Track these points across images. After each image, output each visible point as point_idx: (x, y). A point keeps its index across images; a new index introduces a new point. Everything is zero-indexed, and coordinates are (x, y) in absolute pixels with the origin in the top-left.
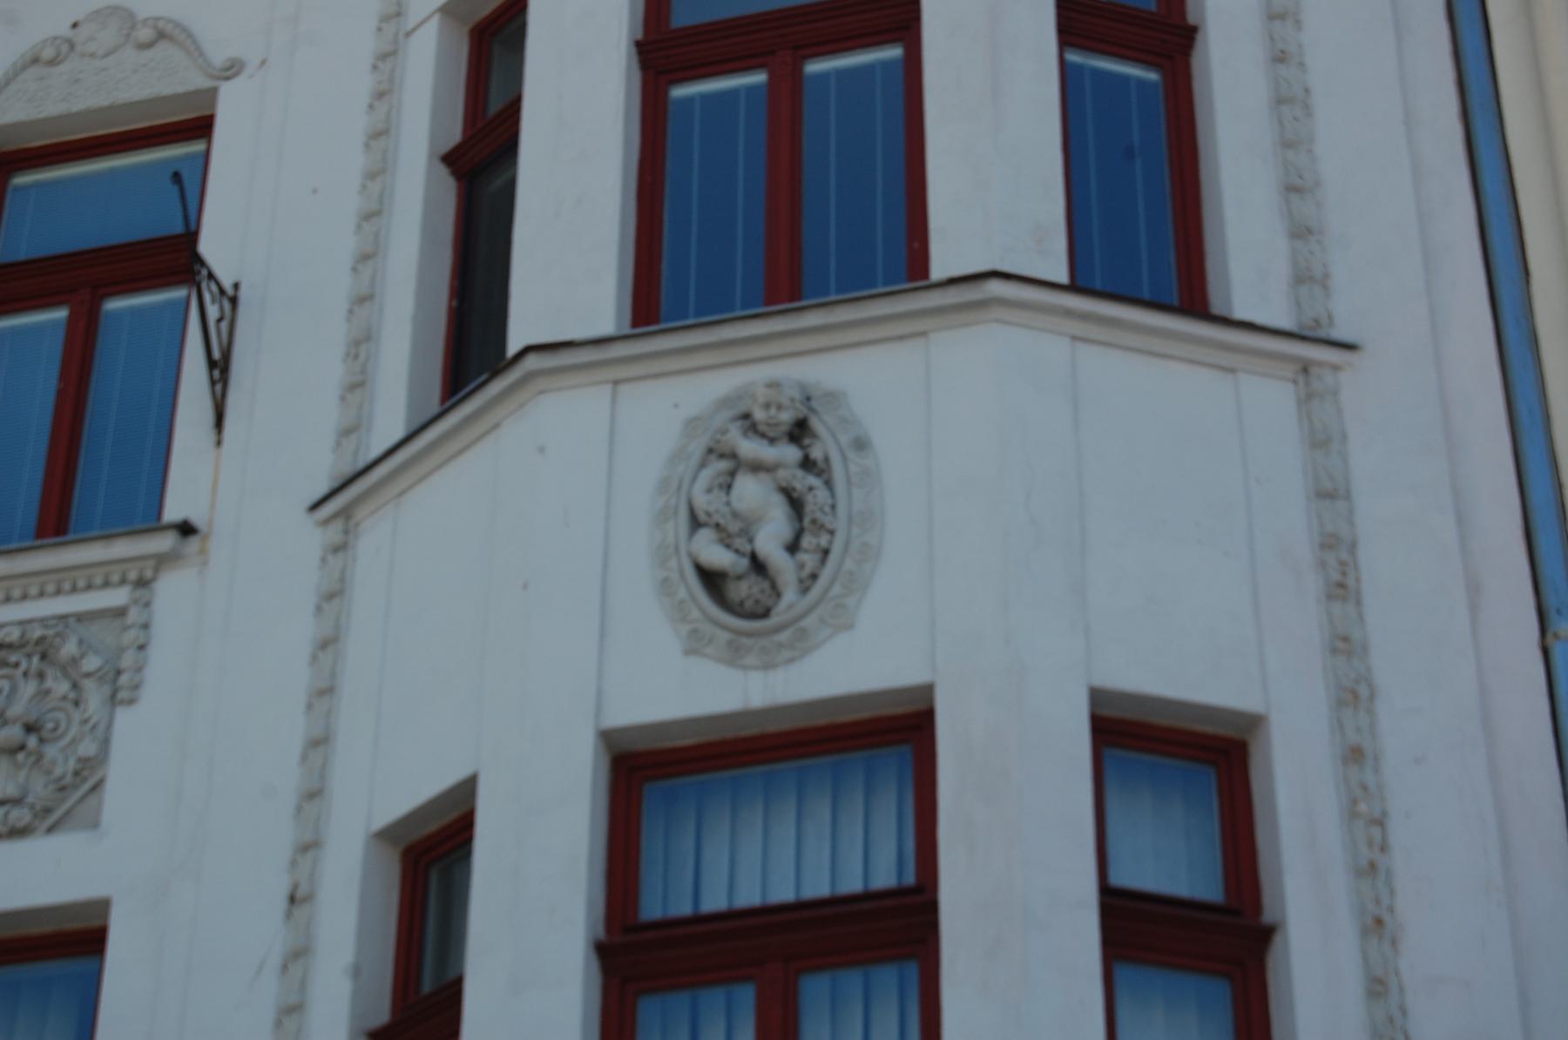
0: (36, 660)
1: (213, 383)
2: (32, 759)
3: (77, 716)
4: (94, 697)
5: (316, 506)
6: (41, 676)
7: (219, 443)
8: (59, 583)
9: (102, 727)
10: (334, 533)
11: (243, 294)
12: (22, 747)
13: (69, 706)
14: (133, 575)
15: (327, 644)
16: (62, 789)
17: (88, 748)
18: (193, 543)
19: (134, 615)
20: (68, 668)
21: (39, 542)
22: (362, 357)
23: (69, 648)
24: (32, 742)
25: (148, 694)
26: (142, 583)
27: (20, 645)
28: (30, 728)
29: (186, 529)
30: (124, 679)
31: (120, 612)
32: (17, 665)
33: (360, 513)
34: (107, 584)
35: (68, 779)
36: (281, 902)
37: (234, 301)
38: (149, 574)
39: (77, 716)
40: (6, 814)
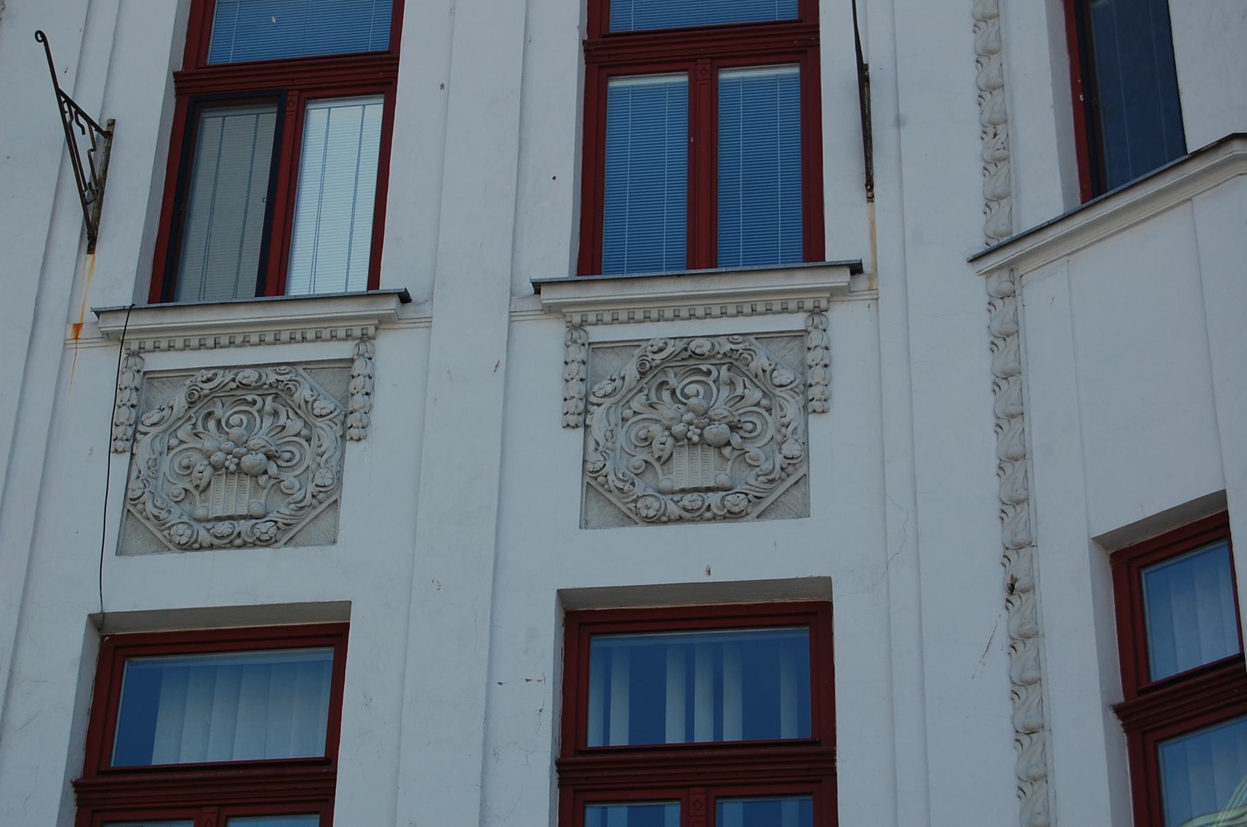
0: (269, 399)
1: (85, 204)
2: (736, 453)
3: (309, 451)
4: (327, 434)
5: (975, 259)
6: (275, 414)
7: (871, 199)
8: (723, 306)
9: (800, 430)
10: (1001, 282)
11: (118, 132)
12: (728, 444)
13: (303, 442)
14: (809, 305)
15: (1007, 377)
16: (771, 481)
17: (324, 477)
18: (861, 282)
19: (359, 367)
20: (305, 411)
21: (806, 265)
22: (1001, 137)
23: (303, 393)
24: (736, 439)
25: (835, 405)
26: (817, 311)
27: (258, 387)
28: (734, 428)
29: (856, 269)
30: (815, 392)
31: (800, 335)
32: (254, 402)
33: (1023, 268)
34: (785, 310)
35: (777, 474)
36: (1000, 593)
37: (108, 135)
38: (823, 304)
39: (309, 451)
40: (723, 498)
